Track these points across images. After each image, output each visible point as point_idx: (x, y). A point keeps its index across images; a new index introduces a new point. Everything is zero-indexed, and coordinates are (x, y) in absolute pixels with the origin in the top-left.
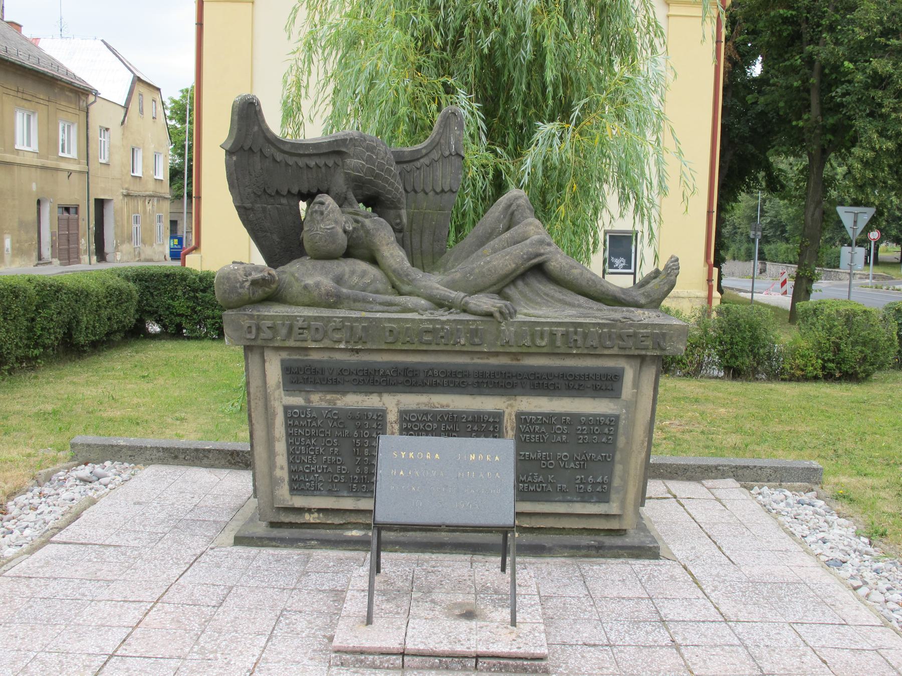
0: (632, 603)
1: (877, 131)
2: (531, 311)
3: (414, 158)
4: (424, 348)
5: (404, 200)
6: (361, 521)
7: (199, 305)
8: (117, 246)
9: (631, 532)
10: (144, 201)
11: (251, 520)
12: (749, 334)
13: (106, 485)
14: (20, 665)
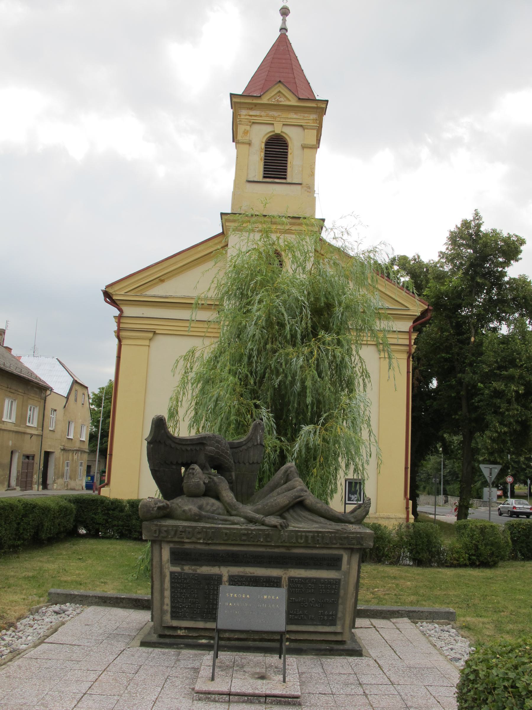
0: (346, 676)
1: (498, 422)
2: (296, 525)
3: (240, 445)
4: (243, 543)
5: (234, 467)
6: (207, 635)
7: (110, 518)
8: (55, 480)
9: (349, 642)
10: (73, 454)
11: (149, 634)
12: (426, 540)
13: (68, 616)
14: (41, 697)
